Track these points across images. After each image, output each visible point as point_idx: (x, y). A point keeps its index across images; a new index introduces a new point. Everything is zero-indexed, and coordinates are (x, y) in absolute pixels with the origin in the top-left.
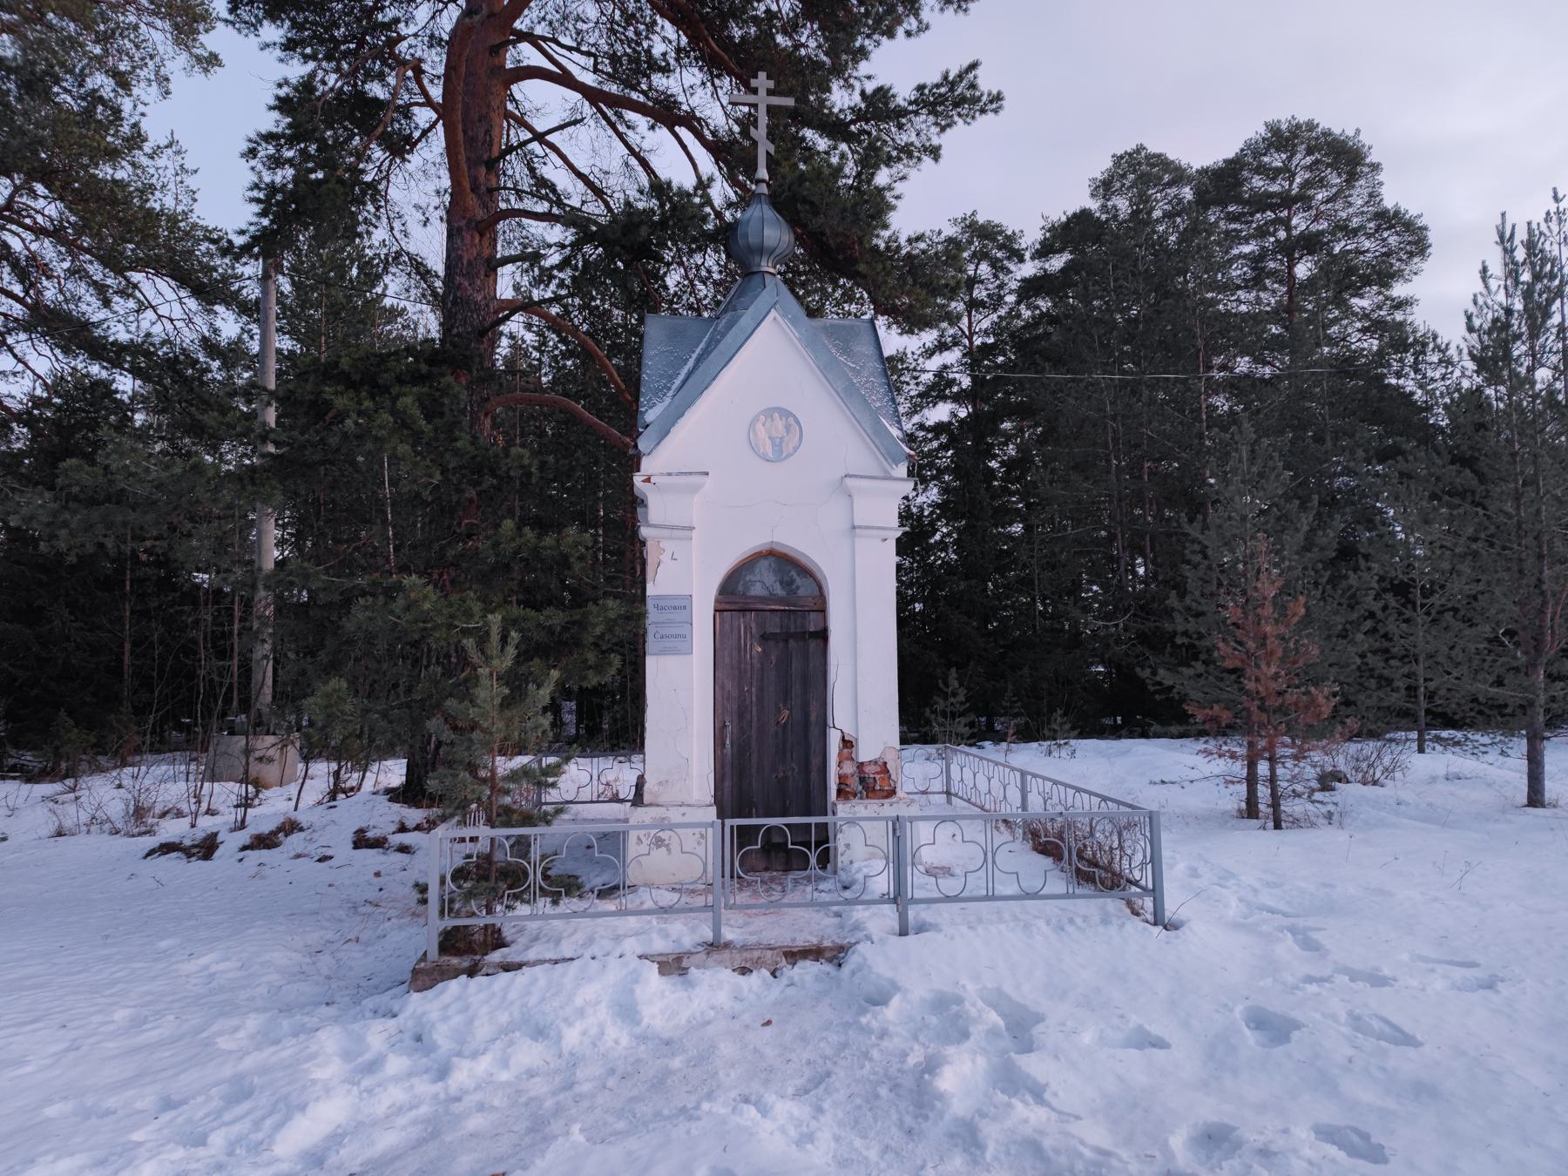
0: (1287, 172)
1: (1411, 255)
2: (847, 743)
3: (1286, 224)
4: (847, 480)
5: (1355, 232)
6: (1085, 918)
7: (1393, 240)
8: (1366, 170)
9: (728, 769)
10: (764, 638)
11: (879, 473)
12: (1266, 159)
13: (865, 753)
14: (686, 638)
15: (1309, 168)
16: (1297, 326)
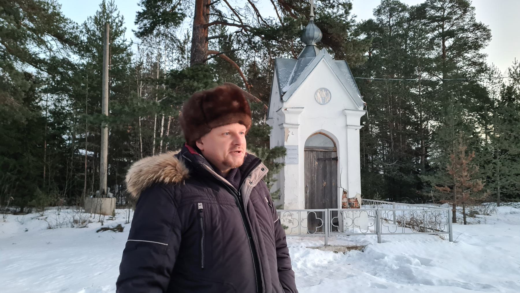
0: (442, 9)
1: (485, 39)
2: (345, 192)
3: (442, 27)
4: (346, 111)
5: (466, 30)
6: (430, 240)
7: (479, 34)
8: (470, 9)
9: (308, 200)
10: (318, 160)
11: (354, 109)
12: (435, 4)
13: (351, 195)
14: (296, 158)
15: (450, 8)
16: (445, 64)
